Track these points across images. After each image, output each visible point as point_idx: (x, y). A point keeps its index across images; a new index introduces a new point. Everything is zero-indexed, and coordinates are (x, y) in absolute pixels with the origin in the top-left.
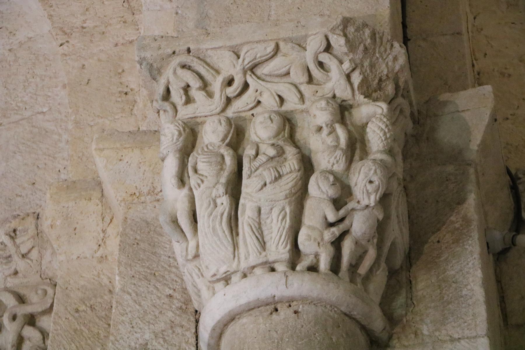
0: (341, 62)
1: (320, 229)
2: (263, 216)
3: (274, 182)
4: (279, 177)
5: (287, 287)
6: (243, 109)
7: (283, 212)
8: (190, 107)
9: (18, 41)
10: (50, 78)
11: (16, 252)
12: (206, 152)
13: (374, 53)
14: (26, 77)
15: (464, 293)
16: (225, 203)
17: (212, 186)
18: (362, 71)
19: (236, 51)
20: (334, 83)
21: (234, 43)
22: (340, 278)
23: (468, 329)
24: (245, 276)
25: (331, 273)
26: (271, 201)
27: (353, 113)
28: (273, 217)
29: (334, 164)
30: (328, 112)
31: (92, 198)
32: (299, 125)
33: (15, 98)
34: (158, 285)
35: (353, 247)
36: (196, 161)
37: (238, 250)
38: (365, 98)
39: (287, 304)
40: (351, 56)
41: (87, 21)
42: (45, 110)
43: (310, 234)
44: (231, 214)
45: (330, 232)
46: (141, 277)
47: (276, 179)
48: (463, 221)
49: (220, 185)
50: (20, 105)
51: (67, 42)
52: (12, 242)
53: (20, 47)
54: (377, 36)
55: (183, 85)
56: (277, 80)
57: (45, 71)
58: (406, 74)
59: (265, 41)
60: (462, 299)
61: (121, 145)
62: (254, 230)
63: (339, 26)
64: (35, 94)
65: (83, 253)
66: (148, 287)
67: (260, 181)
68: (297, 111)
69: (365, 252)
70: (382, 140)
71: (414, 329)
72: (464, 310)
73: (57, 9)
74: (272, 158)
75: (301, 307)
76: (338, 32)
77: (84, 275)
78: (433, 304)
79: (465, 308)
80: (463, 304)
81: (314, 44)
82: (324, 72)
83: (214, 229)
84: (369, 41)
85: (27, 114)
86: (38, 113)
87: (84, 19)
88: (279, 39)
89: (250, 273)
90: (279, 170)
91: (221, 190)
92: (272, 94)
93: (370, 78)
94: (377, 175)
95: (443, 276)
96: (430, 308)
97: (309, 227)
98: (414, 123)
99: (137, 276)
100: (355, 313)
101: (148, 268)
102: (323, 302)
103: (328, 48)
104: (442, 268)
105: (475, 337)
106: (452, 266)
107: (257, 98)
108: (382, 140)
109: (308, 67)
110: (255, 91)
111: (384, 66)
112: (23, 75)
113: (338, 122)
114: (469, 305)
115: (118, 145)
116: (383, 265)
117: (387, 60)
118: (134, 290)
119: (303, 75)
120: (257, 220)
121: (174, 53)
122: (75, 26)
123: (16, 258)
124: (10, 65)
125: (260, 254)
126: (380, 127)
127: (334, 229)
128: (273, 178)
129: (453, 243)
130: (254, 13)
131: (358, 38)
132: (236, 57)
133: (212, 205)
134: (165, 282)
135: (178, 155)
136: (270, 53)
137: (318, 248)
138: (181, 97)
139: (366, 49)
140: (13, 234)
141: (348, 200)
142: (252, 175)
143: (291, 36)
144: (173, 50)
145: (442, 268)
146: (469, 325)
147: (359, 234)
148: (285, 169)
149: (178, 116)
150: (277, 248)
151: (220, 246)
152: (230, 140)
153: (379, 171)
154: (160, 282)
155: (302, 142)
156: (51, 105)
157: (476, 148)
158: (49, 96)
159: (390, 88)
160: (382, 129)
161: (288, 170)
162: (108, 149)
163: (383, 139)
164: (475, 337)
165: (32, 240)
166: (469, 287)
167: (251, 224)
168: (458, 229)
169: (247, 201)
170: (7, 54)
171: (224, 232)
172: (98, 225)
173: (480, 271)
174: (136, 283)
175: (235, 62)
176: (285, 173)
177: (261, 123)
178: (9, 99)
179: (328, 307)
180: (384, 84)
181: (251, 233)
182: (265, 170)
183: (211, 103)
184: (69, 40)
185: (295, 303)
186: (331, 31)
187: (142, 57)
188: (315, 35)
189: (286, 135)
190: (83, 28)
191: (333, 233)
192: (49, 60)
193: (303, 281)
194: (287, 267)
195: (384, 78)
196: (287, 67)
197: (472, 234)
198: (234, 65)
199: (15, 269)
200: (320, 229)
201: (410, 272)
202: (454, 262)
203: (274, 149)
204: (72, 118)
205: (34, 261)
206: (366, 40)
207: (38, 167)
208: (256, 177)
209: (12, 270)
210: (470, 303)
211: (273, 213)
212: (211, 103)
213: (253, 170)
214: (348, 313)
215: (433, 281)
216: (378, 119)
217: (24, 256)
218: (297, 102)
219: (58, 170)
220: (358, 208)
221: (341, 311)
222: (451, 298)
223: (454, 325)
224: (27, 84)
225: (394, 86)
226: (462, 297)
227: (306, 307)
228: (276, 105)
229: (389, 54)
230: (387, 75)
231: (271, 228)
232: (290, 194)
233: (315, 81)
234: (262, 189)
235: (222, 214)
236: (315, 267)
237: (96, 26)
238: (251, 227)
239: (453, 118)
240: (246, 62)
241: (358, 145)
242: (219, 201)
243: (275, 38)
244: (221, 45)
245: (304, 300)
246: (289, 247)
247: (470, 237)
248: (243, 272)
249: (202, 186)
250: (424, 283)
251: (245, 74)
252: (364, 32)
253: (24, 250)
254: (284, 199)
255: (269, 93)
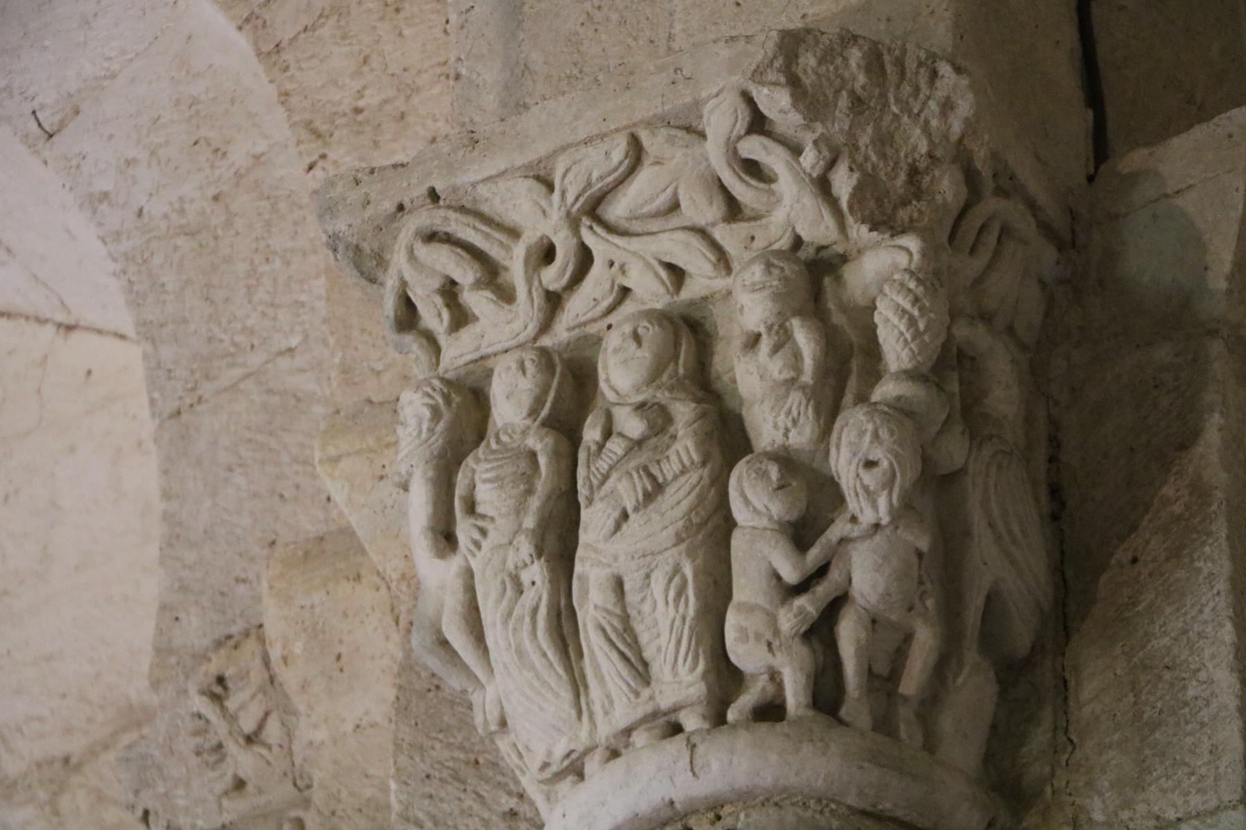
0: (796, 151)
1: (767, 606)
2: (632, 597)
3: (645, 506)
4: (655, 490)
5: (694, 774)
6: (589, 315)
7: (677, 579)
8: (467, 335)
9: (233, 170)
10: (304, 254)
11: (230, 733)
12: (493, 452)
13: (886, 105)
14: (252, 262)
15: (1191, 693)
16: (539, 583)
17: (506, 541)
18: (853, 160)
19: (542, 173)
20: (788, 209)
21: (530, 156)
22: (841, 722)
23: (1198, 791)
24: (615, 754)
25: (811, 713)
26: (644, 556)
27: (846, 275)
28: (655, 595)
29: (787, 430)
30: (766, 293)
31: (363, 573)
32: (721, 332)
33: (230, 322)
34: (484, 789)
35: (863, 635)
36: (473, 480)
37: (587, 695)
38: (871, 230)
39: (711, 815)
40: (820, 129)
41: (367, 92)
42: (294, 342)
43: (744, 624)
44: (559, 604)
45: (791, 610)
46: (445, 774)
47: (649, 497)
48: (1191, 494)
49: (523, 537)
50: (239, 339)
51: (323, 157)
52: (218, 710)
53: (237, 185)
54: (887, 58)
55: (436, 283)
56: (655, 226)
57: (293, 239)
58: (986, 137)
59: (602, 137)
60: (1187, 710)
61: (379, 439)
62: (613, 636)
63: (772, 62)
64: (272, 305)
65: (367, 713)
66: (460, 799)
67: (610, 511)
68: (717, 296)
69: (908, 638)
70: (906, 341)
71: (1069, 812)
72: (1189, 740)
73: (298, 74)
74: (639, 443)
75: (742, 816)
76: (772, 76)
77: (371, 771)
78: (1116, 737)
79: (1191, 734)
80: (1187, 723)
81: (722, 119)
82: (761, 185)
83: (520, 653)
84: (862, 79)
85: (255, 360)
86: (281, 353)
87: (358, 87)
88: (634, 125)
89: (627, 747)
90: (655, 471)
91: (525, 547)
92: (648, 265)
93: (882, 173)
94: (881, 443)
95: (1141, 654)
96: (1110, 747)
97: (749, 609)
98: (1060, 249)
99: (437, 774)
100: (888, 805)
101: (461, 748)
102: (795, 795)
103: (758, 124)
104: (1141, 633)
105: (1214, 812)
106: (1165, 624)
107: (617, 282)
108: (906, 341)
109: (720, 180)
110: (607, 264)
111: (918, 131)
112: (244, 260)
113: (799, 313)
114: (1203, 725)
115: (371, 441)
116: (971, 655)
117: (923, 115)
118: (428, 813)
119: (711, 203)
120: (618, 611)
121: (401, 208)
122: (340, 109)
123: (233, 748)
124: (216, 238)
125: (637, 694)
126: (899, 305)
127: (801, 601)
128: (641, 497)
129: (1167, 560)
130: (635, 39)
131: (828, 79)
132: (543, 189)
133: (510, 593)
134: (499, 778)
135: (430, 474)
136: (621, 163)
137: (770, 655)
138: (440, 315)
139: (858, 103)
140: (218, 689)
141: (835, 514)
142: (596, 497)
143: (659, 110)
144: (397, 200)
145: (1141, 633)
146: (1202, 778)
147: (874, 599)
148: (670, 468)
149: (442, 365)
150: (675, 674)
151: (544, 691)
152: (553, 408)
153: (886, 430)
154: (487, 782)
155: (726, 378)
156: (307, 326)
157: (1223, 285)
158: (303, 304)
159: (947, 187)
160: (904, 311)
161: (676, 467)
162: (349, 455)
163: (908, 336)
164: (1214, 812)
165: (260, 696)
166: (1203, 675)
167: (604, 623)
168: (1179, 518)
169: (588, 564)
170: (209, 211)
171: (545, 655)
172: (387, 638)
173: (1229, 626)
174: (433, 792)
175: (543, 203)
176: (669, 477)
177: (616, 351)
178: (216, 330)
179: (812, 802)
180: (927, 179)
181: (606, 647)
182: (619, 480)
183: (510, 316)
184: (326, 151)
185: (728, 809)
186: (753, 78)
187: (331, 233)
188: (717, 95)
189: (681, 371)
190: (358, 111)
191: (801, 610)
192: (301, 207)
193: (732, 751)
194: (704, 717)
195: (922, 165)
196: (669, 191)
197: (1214, 528)
198: (544, 212)
199: (236, 777)
200: (767, 606)
201: (1063, 654)
202: (1168, 610)
203: (642, 418)
204: (337, 360)
205: (276, 749)
206: (854, 79)
207: (282, 496)
208: (602, 499)
209: (228, 779)
210: (1206, 720)
211: (653, 585)
212: (510, 316)
213: (595, 482)
214: (869, 809)
215: (1118, 672)
216: (896, 285)
217: (250, 740)
218: (711, 274)
219: (324, 497)
220: (855, 534)
221: (849, 807)
222: (1161, 712)
223: (1165, 786)
224: (254, 282)
225: (960, 176)
226: (1186, 704)
227: (755, 815)
228: (662, 290)
229: (929, 98)
230: (930, 155)
231: (656, 624)
232: (686, 528)
233: (747, 212)
234: (618, 527)
235: (535, 611)
236: (777, 702)
237: (386, 102)
238: (604, 631)
239: (1154, 216)
240: (570, 198)
241: (855, 364)
242: (525, 577)
243: (625, 123)
244: (502, 168)
245: (745, 798)
246: (701, 666)
247: (1209, 534)
248: (607, 748)
249: (485, 544)
250: (1096, 685)
251: (574, 223)
252: (845, 59)
253: (248, 725)
254: (675, 545)
255: (641, 264)
